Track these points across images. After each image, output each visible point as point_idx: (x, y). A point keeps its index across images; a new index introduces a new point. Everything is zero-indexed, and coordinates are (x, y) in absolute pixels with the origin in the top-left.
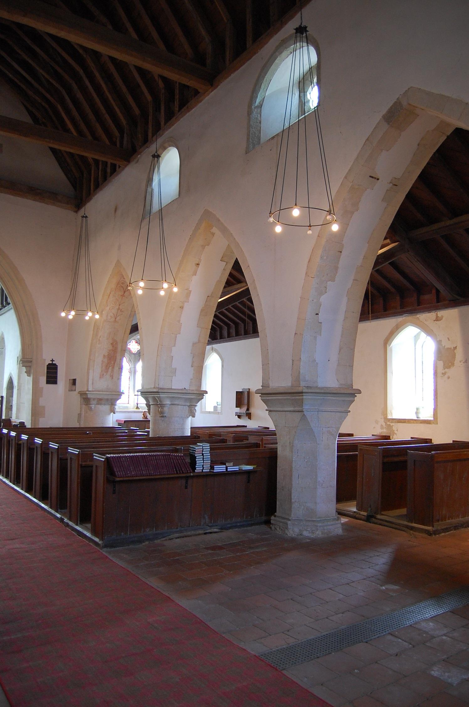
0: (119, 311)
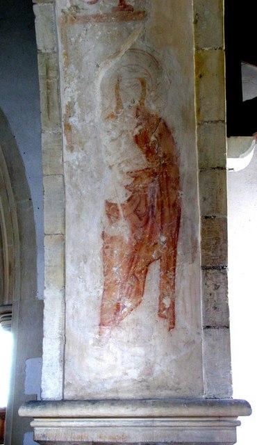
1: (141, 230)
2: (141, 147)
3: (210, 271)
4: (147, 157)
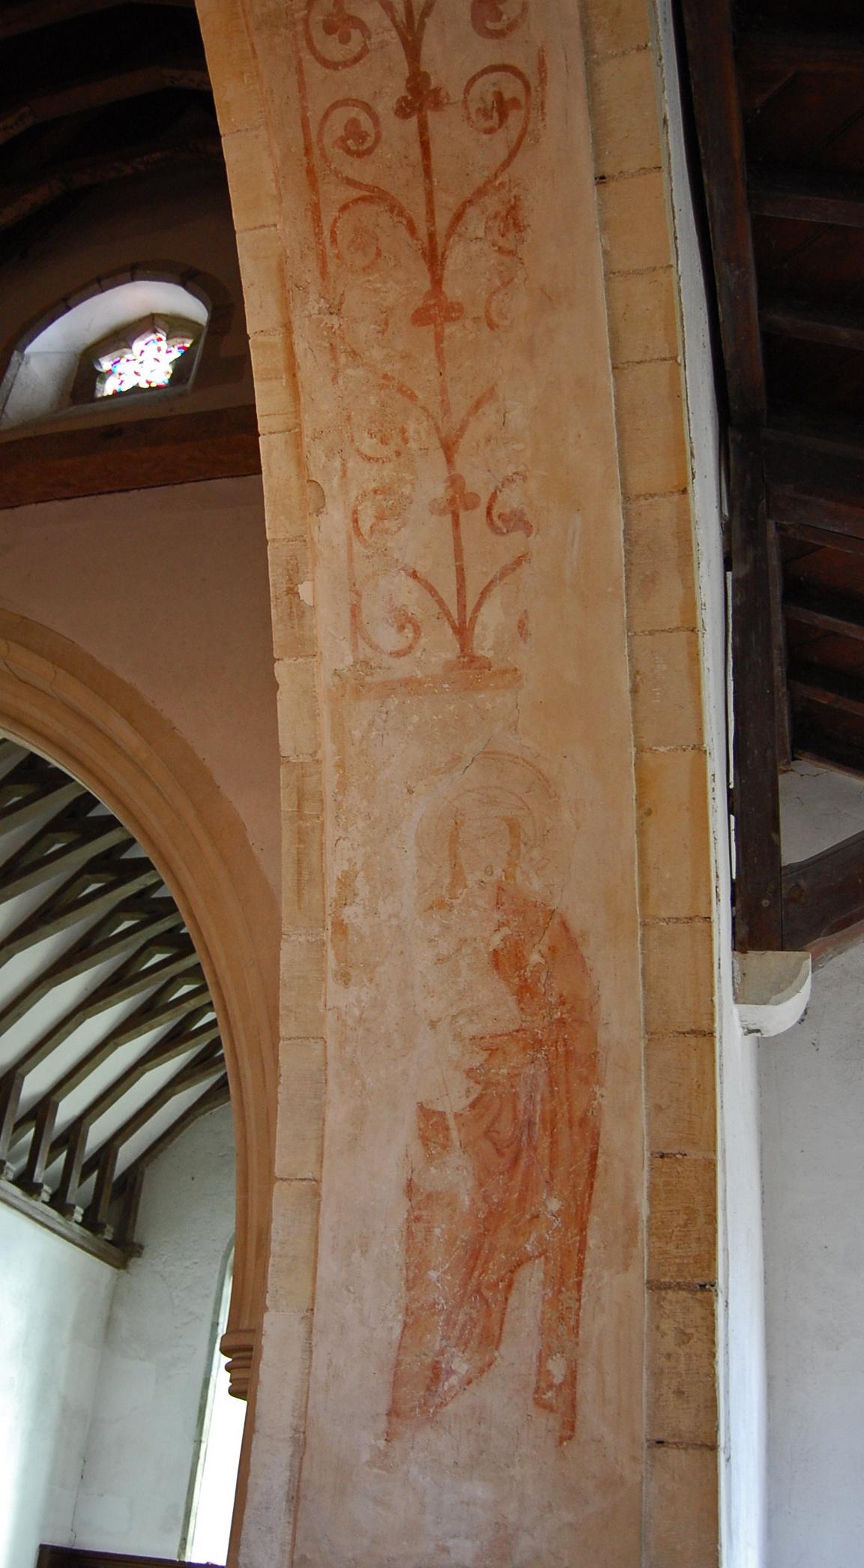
0: (474, 521)
2: (506, 979)
3: (670, 1295)
4: (519, 1001)
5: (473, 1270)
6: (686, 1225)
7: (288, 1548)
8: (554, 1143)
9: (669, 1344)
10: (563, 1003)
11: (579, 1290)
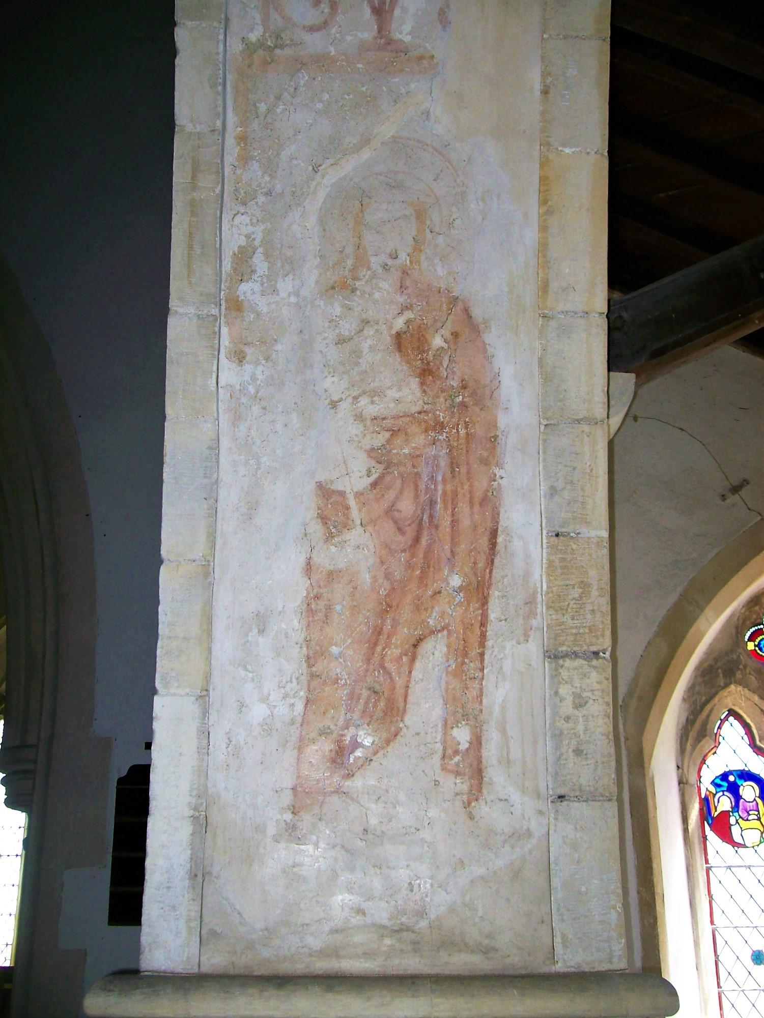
1: (403, 557)
2: (408, 362)
3: (568, 663)
4: (422, 384)
5: (376, 644)
6: (581, 597)
7: (195, 924)
8: (454, 522)
9: (567, 708)
10: (464, 387)
11: (482, 661)
